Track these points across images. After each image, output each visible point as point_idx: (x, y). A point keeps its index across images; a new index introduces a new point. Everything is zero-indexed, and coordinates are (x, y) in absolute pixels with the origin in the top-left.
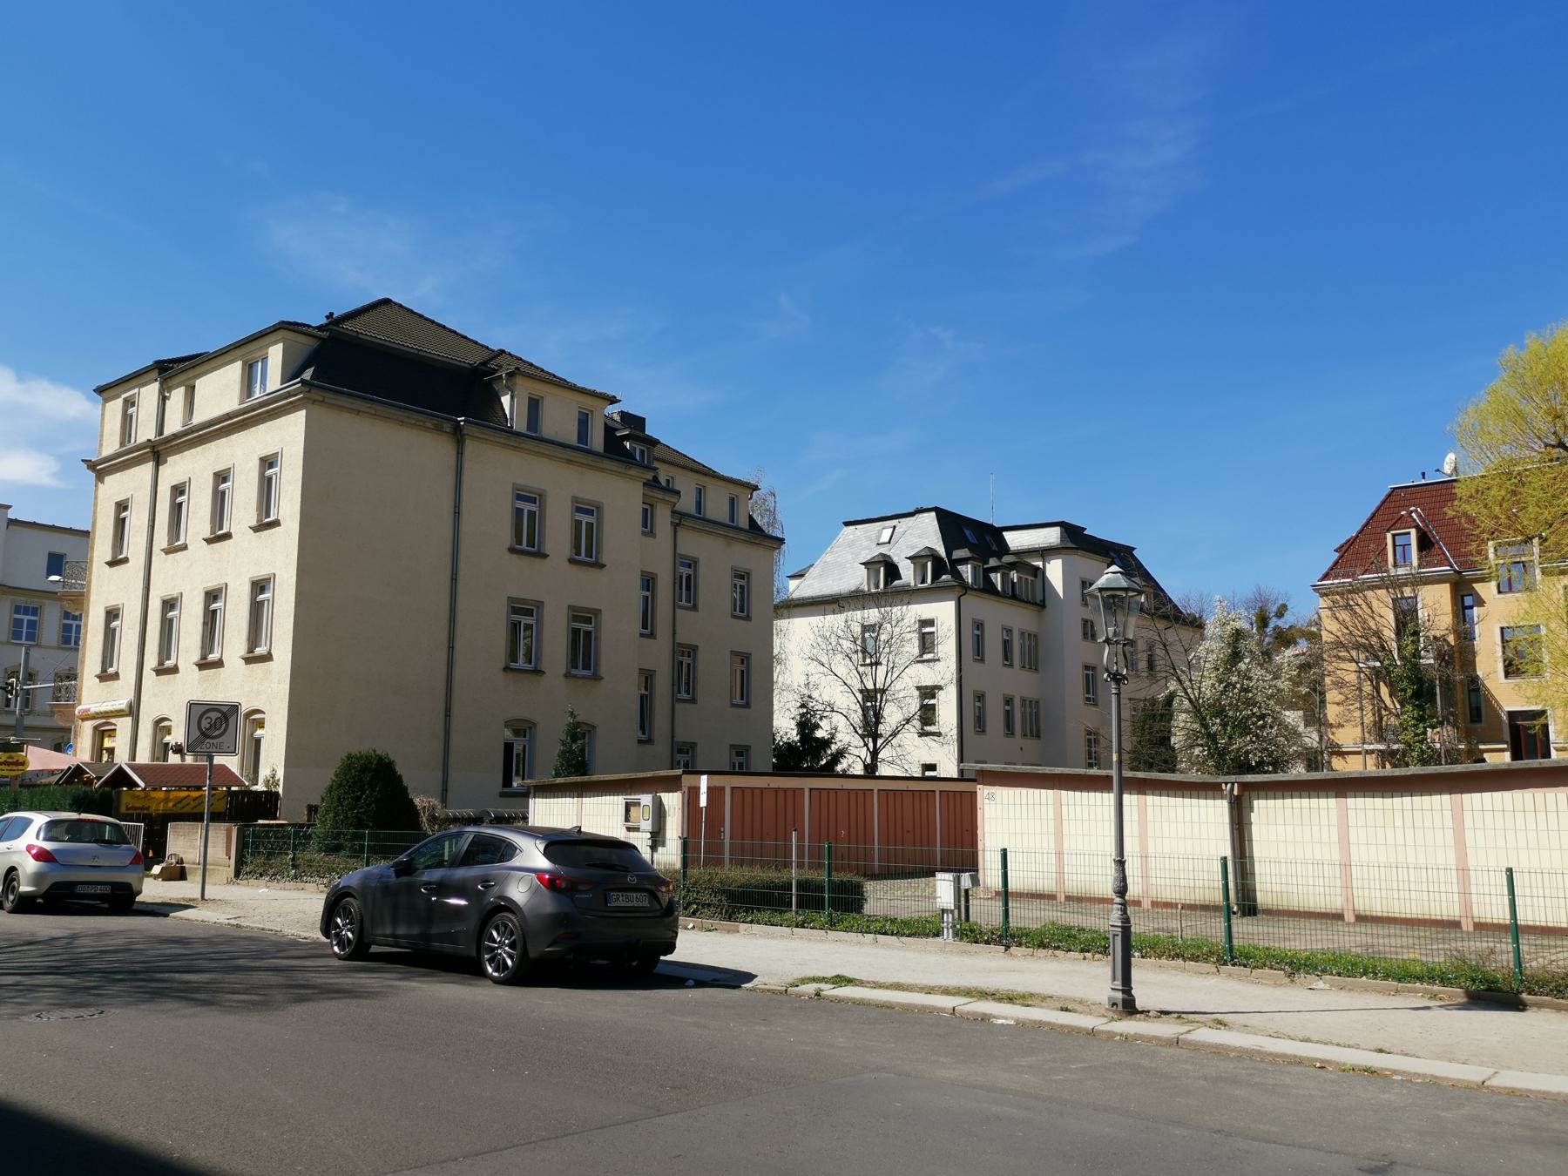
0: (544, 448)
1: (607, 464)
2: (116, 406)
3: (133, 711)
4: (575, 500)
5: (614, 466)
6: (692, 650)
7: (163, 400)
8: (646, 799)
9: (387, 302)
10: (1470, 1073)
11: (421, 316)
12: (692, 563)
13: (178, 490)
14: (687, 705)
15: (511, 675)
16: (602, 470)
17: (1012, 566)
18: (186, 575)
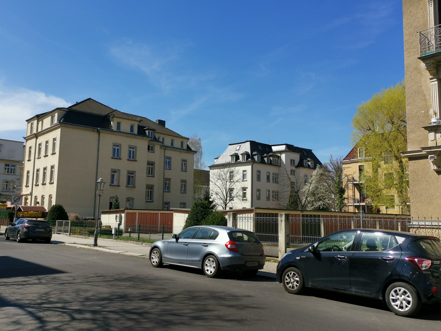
0: (121, 134)
1: (138, 137)
2: (30, 124)
3: (31, 194)
4: (129, 145)
5: (140, 137)
6: (169, 179)
7: (38, 124)
8: (118, 215)
9: (90, 99)
10: (118, 252)
11: (98, 102)
12: (170, 158)
13: (40, 145)
14: (168, 193)
15: (112, 187)
16: (136, 138)
17: (271, 156)
18: (41, 164)
